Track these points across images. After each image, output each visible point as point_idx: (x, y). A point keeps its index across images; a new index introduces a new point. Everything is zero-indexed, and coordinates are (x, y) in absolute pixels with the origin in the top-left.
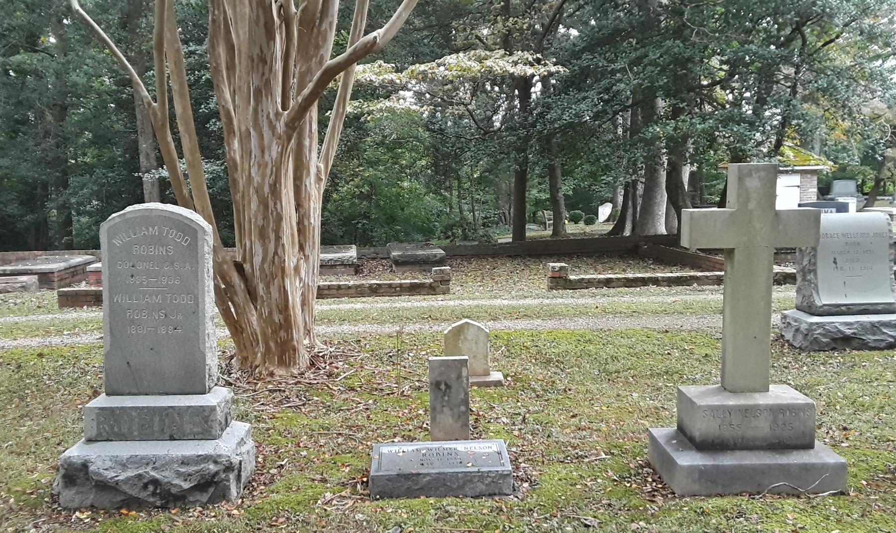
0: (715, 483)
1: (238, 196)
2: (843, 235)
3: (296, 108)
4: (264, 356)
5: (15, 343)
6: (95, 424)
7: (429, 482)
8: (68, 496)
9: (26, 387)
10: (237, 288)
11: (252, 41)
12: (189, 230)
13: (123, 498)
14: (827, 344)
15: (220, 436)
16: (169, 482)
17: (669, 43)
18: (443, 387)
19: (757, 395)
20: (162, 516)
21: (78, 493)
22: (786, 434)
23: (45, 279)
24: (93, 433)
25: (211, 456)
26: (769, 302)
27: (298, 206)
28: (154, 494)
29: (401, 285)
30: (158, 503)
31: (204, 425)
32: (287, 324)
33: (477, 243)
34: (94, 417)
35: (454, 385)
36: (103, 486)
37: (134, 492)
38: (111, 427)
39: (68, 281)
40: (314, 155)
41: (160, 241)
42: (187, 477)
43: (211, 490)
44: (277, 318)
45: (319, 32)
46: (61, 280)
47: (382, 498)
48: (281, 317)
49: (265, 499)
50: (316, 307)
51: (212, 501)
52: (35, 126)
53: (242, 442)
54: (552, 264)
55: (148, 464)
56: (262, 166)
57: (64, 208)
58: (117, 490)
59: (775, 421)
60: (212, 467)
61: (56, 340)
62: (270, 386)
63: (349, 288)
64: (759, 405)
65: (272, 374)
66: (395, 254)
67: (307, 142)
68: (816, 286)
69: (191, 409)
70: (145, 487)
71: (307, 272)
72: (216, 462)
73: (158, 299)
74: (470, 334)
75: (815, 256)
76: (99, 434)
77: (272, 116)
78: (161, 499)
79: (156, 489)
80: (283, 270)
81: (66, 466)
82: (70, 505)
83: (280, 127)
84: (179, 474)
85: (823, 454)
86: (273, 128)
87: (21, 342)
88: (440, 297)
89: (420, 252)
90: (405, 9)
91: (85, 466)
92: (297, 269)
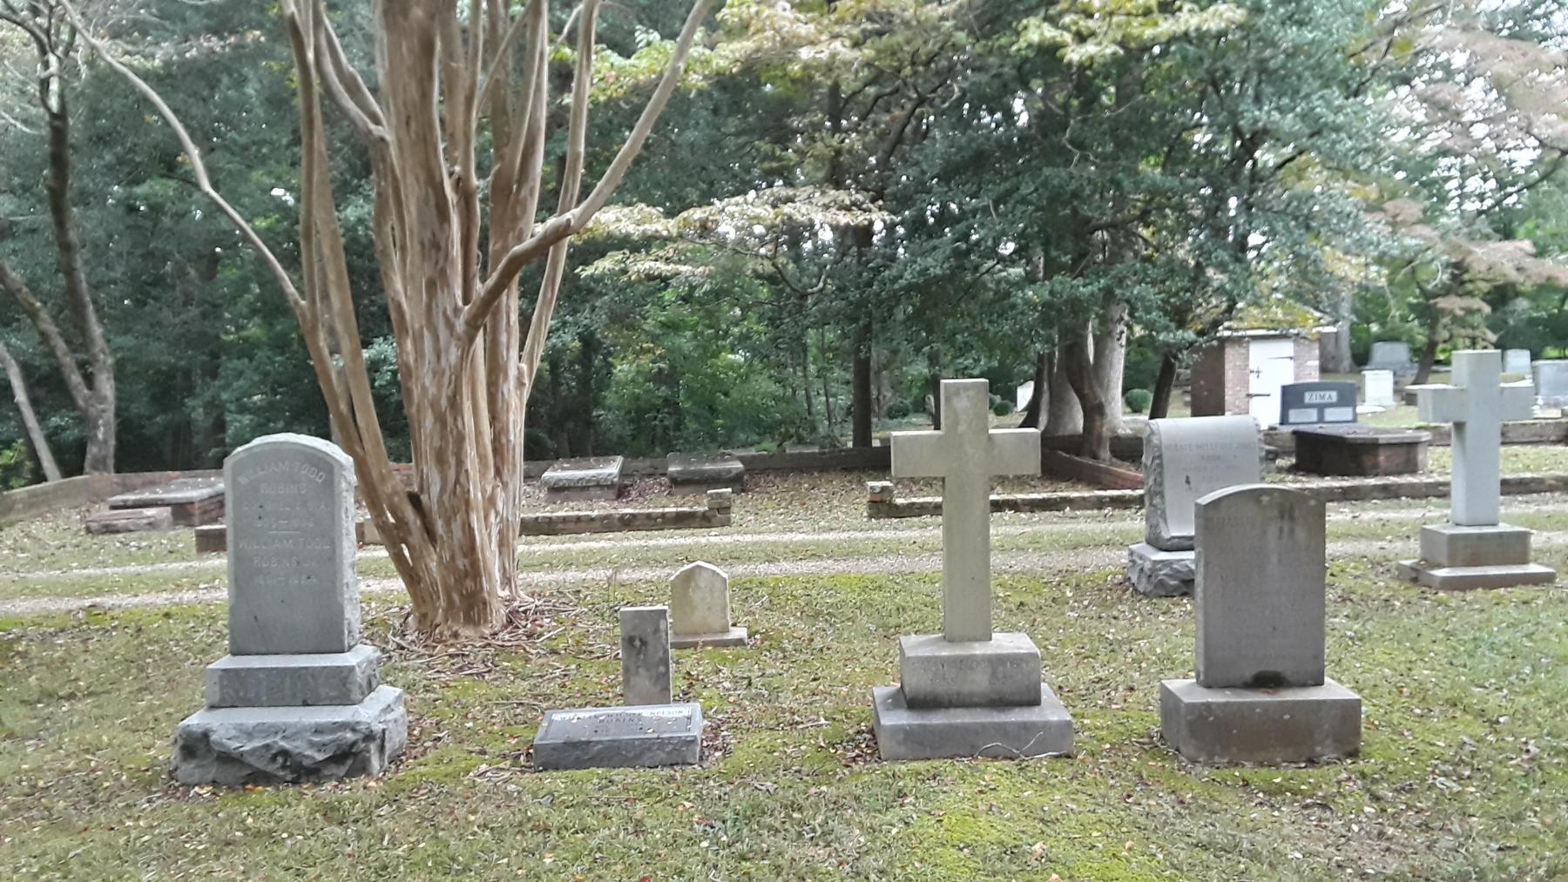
0: (922, 745)
1: (414, 409)
2: (1199, 447)
4: (446, 611)
5: (136, 600)
6: (217, 688)
7: (600, 751)
8: (188, 769)
9: (149, 654)
10: (413, 527)
11: (423, 224)
12: (325, 465)
14: (1176, 588)
15: (361, 701)
17: (1047, 171)
18: (637, 643)
19: (977, 645)
20: (291, 790)
21: (197, 767)
22: (1008, 688)
23: (182, 512)
24: (216, 699)
26: (987, 537)
27: (494, 419)
28: (283, 767)
29: (663, 515)
31: (341, 688)
32: (474, 571)
33: (816, 450)
35: (650, 639)
36: (227, 758)
37: (260, 765)
38: (236, 691)
39: (214, 514)
40: (514, 353)
42: (321, 747)
43: (350, 762)
44: (461, 562)
45: (517, 201)
46: (205, 512)
47: (545, 770)
48: (466, 561)
49: (410, 771)
50: (521, 548)
51: (351, 774)
52: (173, 287)
53: (388, 709)
54: (871, 484)
56: (437, 374)
57: (214, 405)
59: (994, 674)
60: (349, 736)
61: (188, 596)
62: (452, 650)
63: (592, 519)
64: (975, 656)
65: (456, 635)
66: (672, 469)
67: (504, 338)
68: (1164, 512)
70: (274, 758)
71: (506, 503)
72: (354, 730)
74: (703, 580)
75: (1161, 474)
76: (223, 699)
77: (449, 312)
80: (467, 503)
82: (189, 780)
83: (460, 326)
84: (312, 744)
85: (1052, 710)
86: (450, 326)
87: (145, 598)
88: (714, 531)
89: (708, 467)
90: (607, 183)
91: (206, 735)
92: (491, 501)
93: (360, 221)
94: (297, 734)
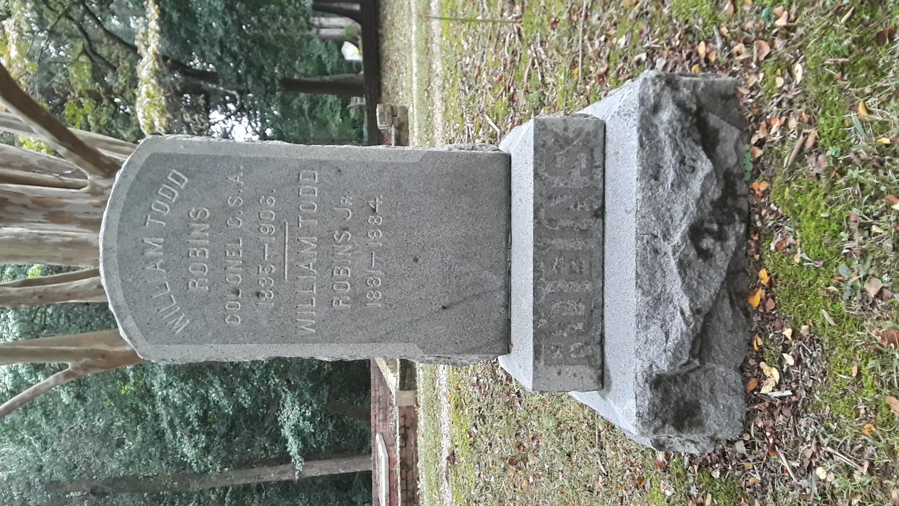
3: (77, 157)
6: (569, 370)
8: (720, 417)
13: (726, 303)
16: (698, 202)
21: (713, 400)
24: (588, 373)
25: (643, 117)
28: (721, 237)
30: (741, 229)
34: (554, 371)
36: (701, 343)
37: (716, 278)
38: (575, 339)
41: (177, 237)
42: (685, 167)
55: (656, 252)
58: (709, 316)
60: (667, 114)
69: (541, 171)
72: (656, 109)
73: (309, 243)
78: (731, 222)
79: (710, 232)
81: (658, 423)
84: (680, 183)
91: (658, 382)
93: (195, 446)
94: (656, 211)
